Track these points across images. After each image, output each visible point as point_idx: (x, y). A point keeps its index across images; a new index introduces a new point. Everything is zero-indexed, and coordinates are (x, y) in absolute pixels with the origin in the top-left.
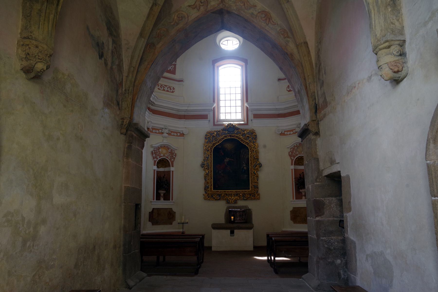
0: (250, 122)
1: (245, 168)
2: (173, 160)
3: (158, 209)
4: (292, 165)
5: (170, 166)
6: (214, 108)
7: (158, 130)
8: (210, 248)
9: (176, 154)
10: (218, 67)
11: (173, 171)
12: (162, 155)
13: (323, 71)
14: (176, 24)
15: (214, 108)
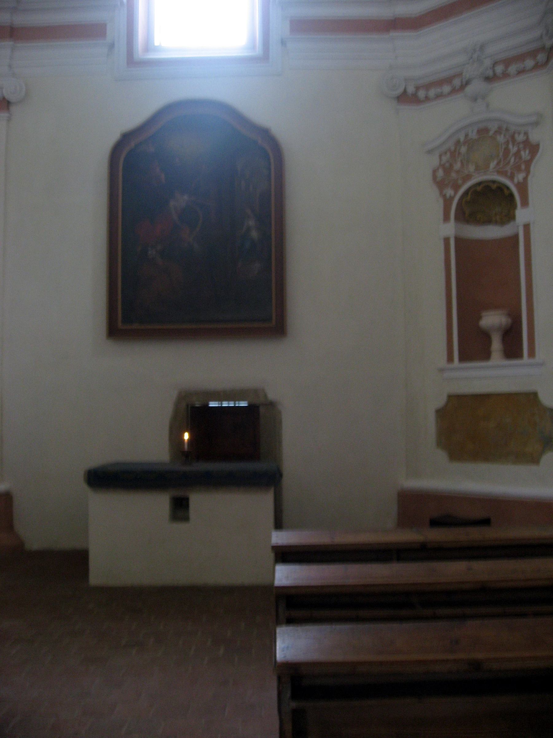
1: (254, 234)
4: (446, 218)
10: (148, 47)
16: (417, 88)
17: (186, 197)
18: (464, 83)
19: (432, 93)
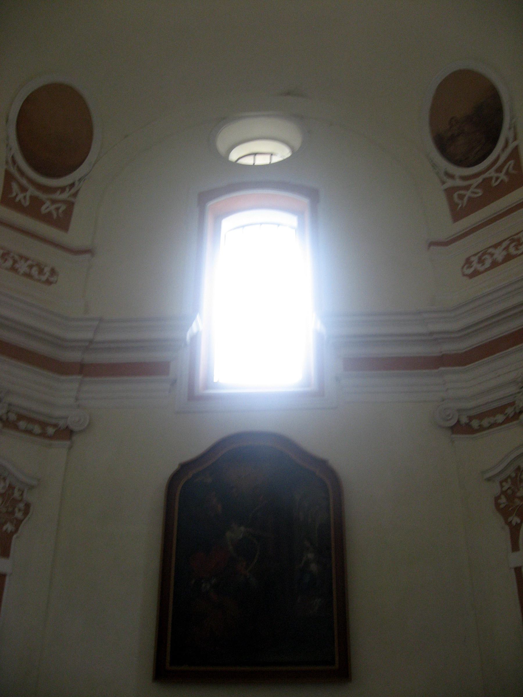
1: (314, 567)
9: (28, 506)
10: (218, 218)
16: (471, 418)
17: (242, 528)
18: (518, 411)
19: (485, 423)
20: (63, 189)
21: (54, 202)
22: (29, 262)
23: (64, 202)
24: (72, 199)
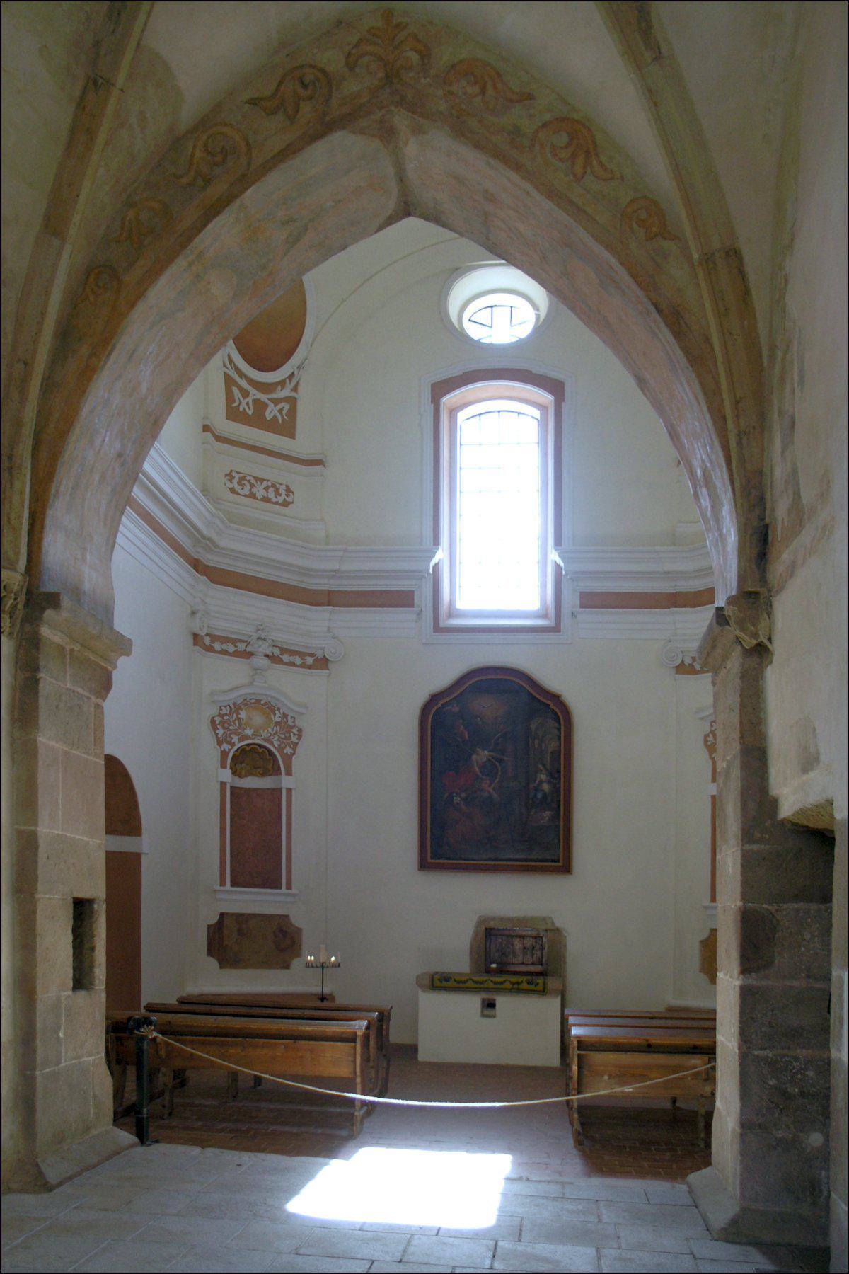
0: (566, 621)
2: (288, 750)
3: (242, 919)
5: (278, 772)
6: (436, 566)
7: (234, 641)
8: (412, 1049)
9: (300, 730)
11: (289, 791)
12: (249, 732)
13: (796, 378)
14: (200, 182)
15: (436, 566)
20: (282, 384)
21: (276, 402)
22: (265, 484)
23: (286, 399)
24: (294, 394)
